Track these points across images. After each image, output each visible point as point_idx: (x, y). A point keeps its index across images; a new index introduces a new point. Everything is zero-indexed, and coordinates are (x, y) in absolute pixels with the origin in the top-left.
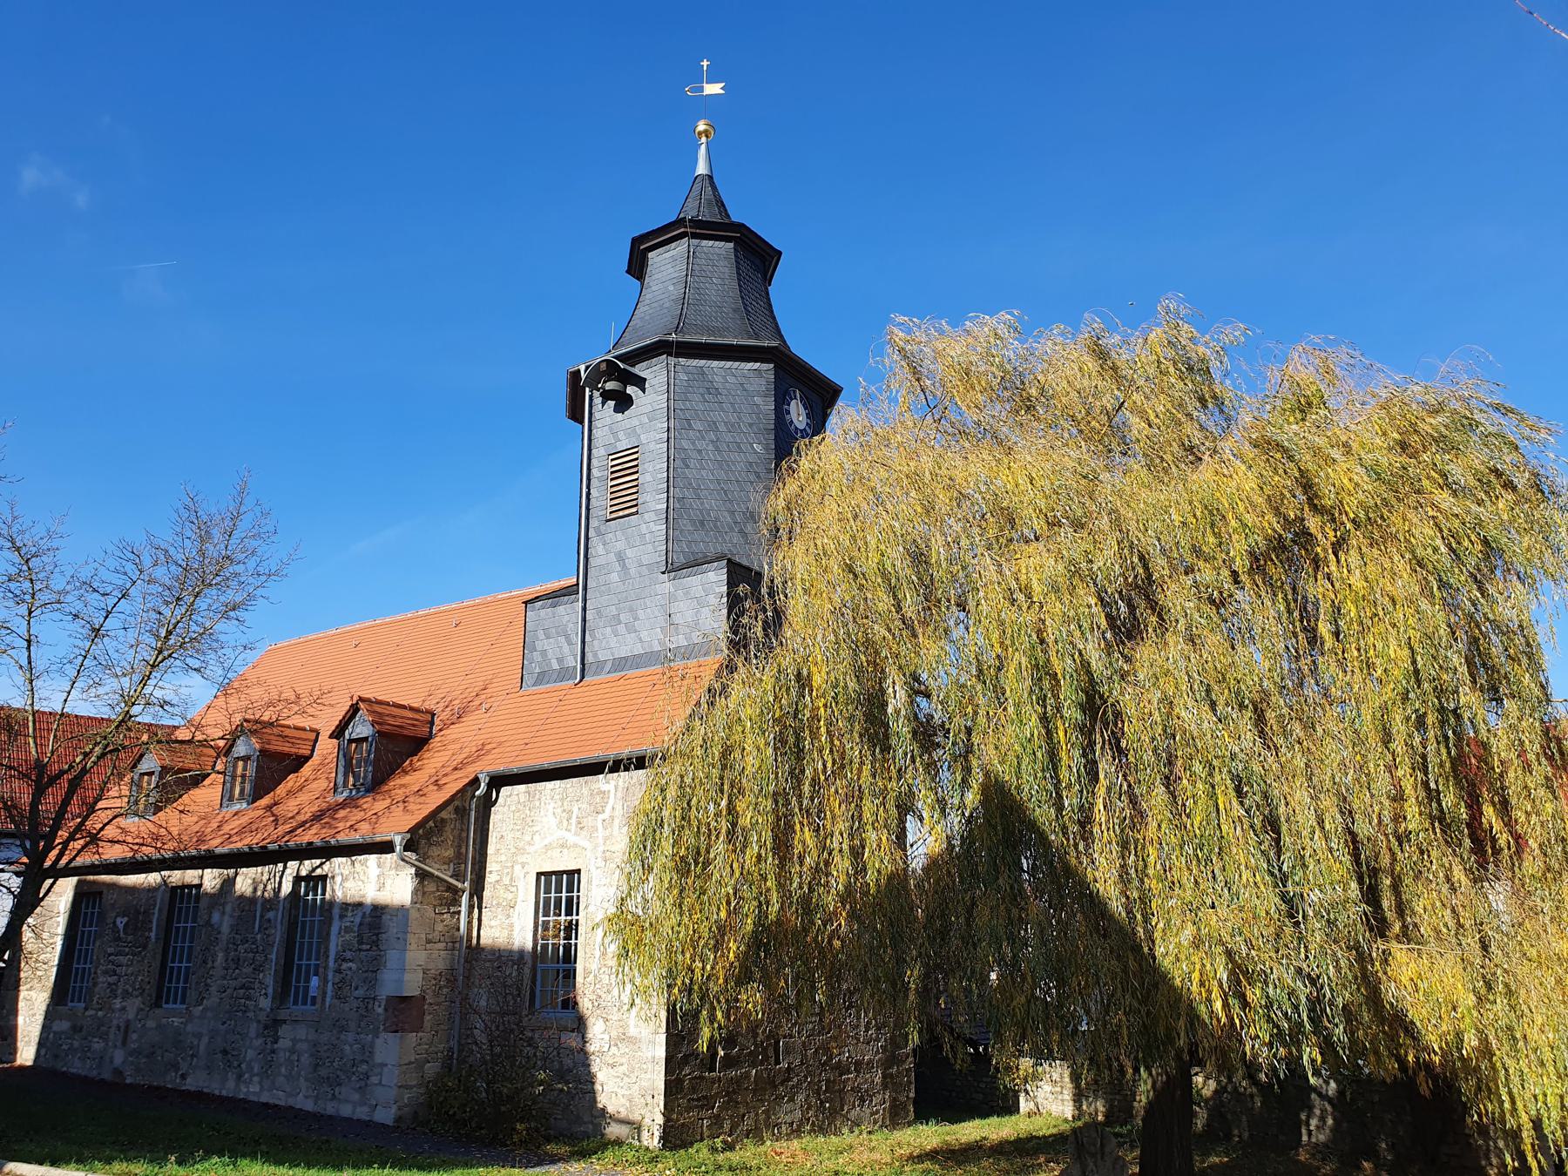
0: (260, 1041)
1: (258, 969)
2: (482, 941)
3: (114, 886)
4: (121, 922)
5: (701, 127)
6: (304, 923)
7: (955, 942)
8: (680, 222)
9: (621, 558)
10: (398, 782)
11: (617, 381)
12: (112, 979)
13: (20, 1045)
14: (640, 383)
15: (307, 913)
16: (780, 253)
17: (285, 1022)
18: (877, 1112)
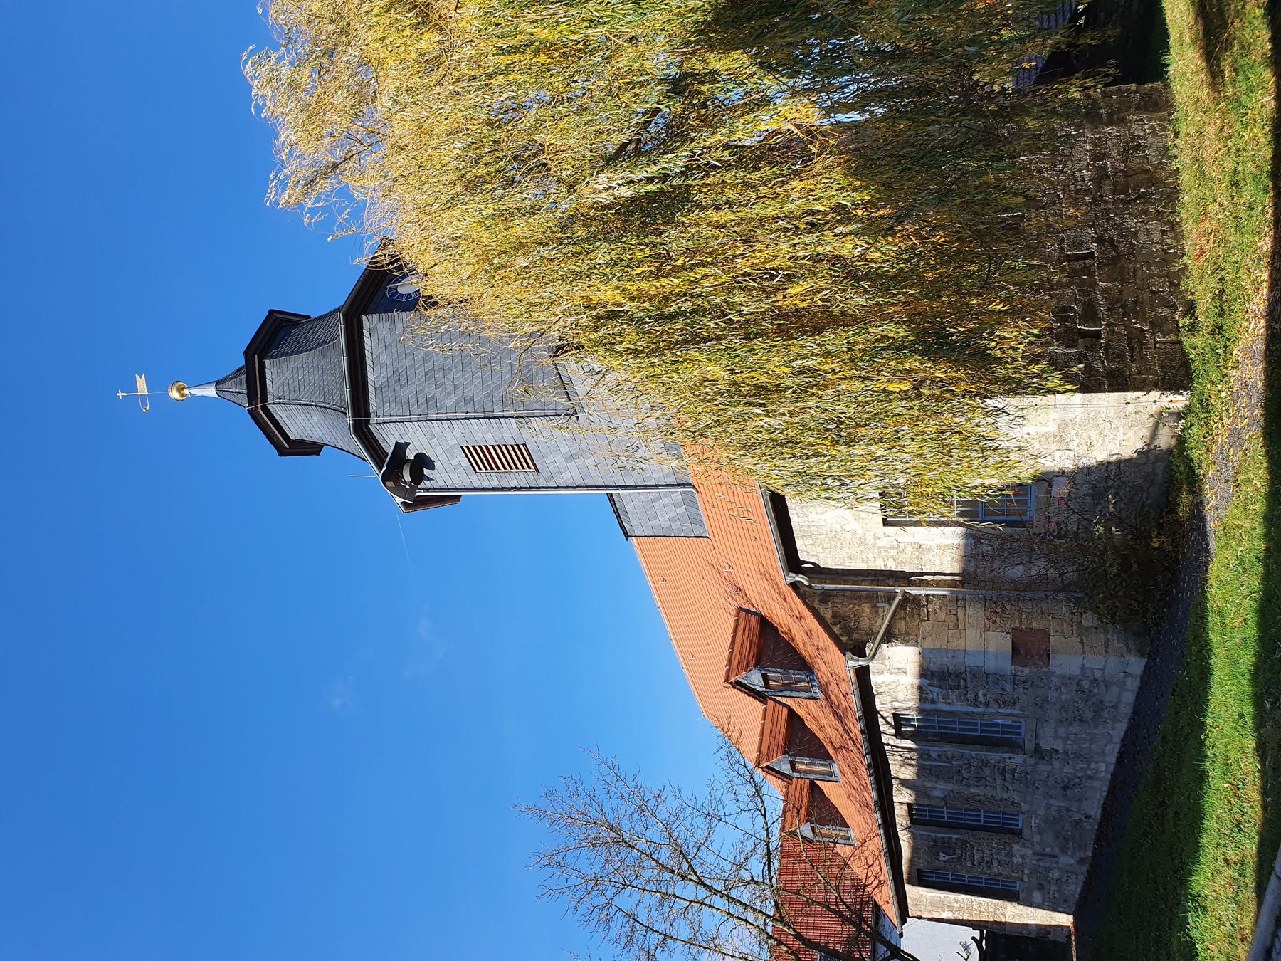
0: (1055, 762)
1: (986, 763)
2: (957, 571)
3: (911, 861)
4: (942, 857)
5: (175, 395)
6: (940, 728)
7: (932, 74)
8: (253, 414)
9: (570, 457)
10: (801, 647)
11: (402, 469)
12: (995, 864)
13: (1054, 923)
14: (401, 448)
15: (929, 730)
16: (271, 312)
17: (1037, 745)
18: (1152, 128)
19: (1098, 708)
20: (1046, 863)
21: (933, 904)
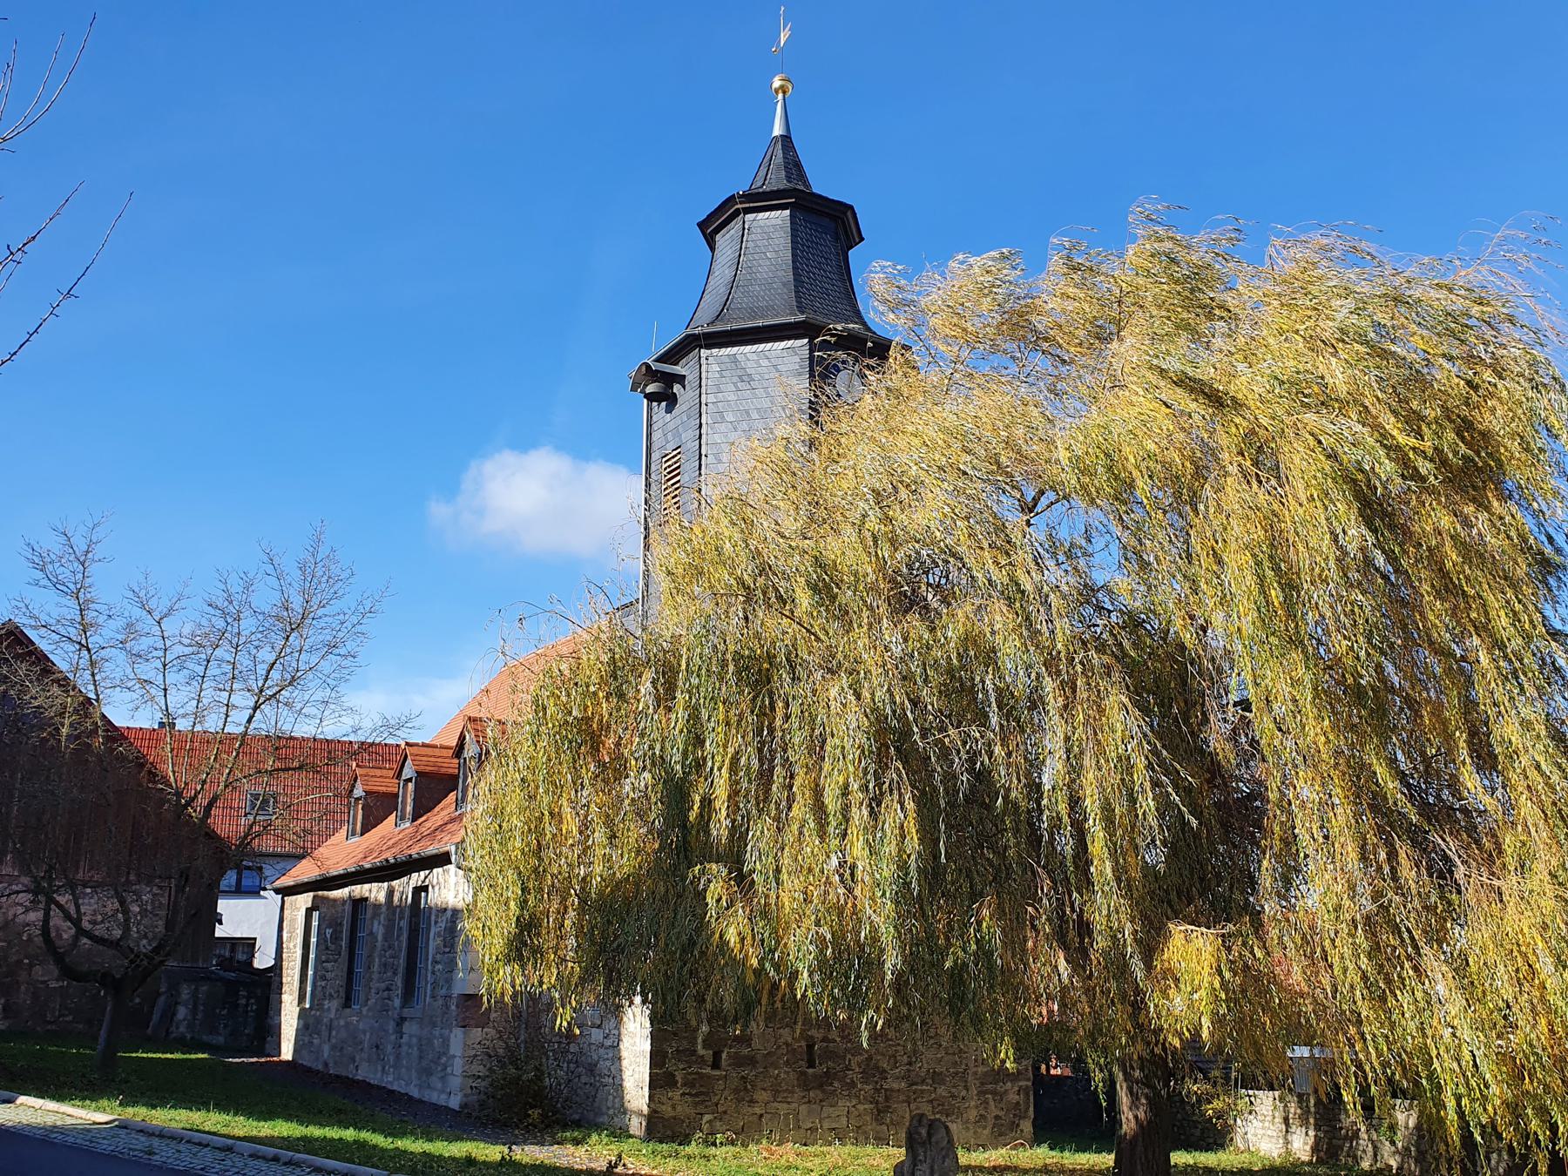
1: (395, 974)
5: (777, 83)
8: (730, 200)
19: (428, 1072)
20: (325, 1034)
21: (293, 920)
